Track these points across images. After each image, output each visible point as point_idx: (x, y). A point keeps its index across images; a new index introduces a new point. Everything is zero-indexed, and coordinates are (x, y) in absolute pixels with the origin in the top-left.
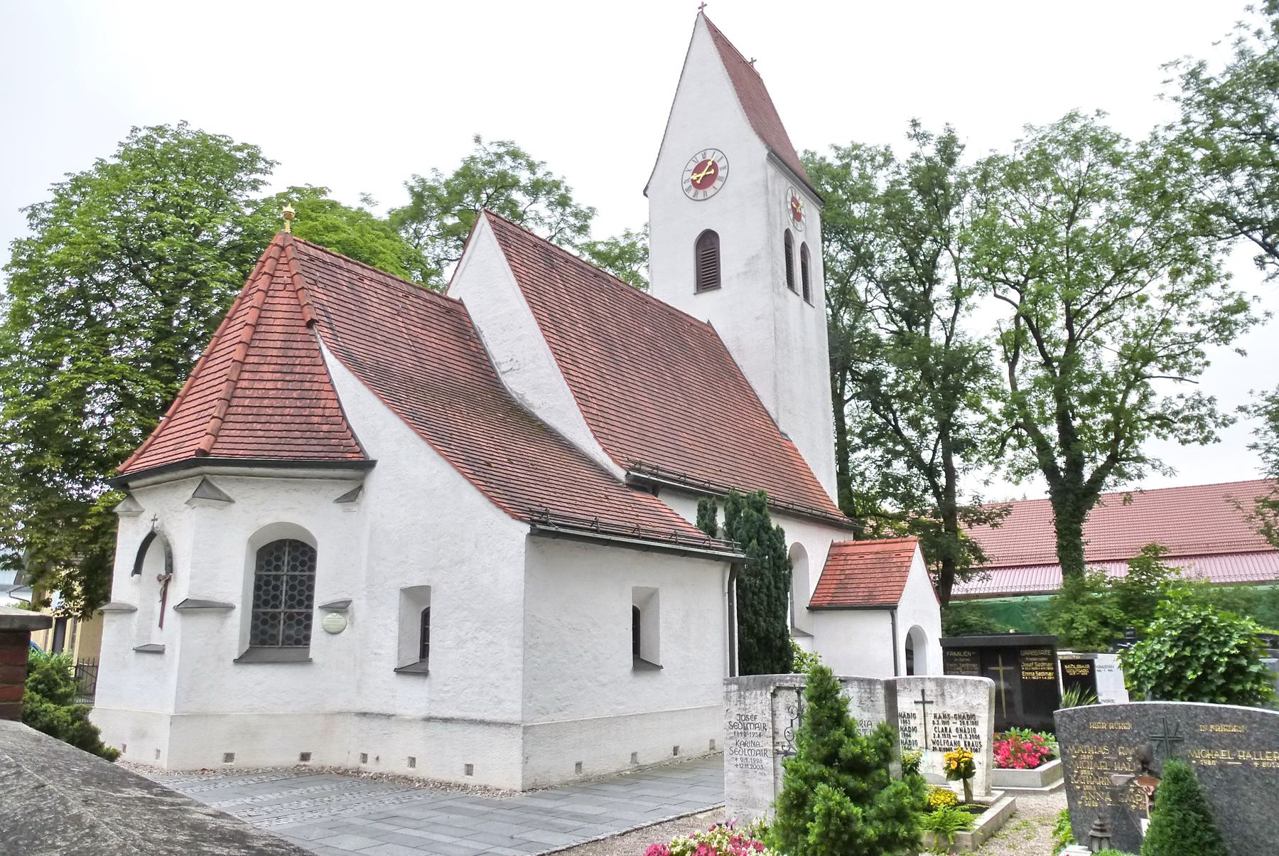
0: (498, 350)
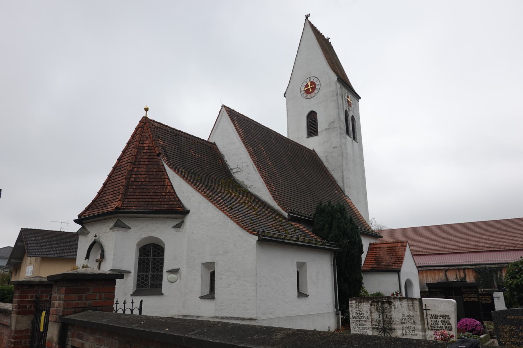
0: (232, 162)
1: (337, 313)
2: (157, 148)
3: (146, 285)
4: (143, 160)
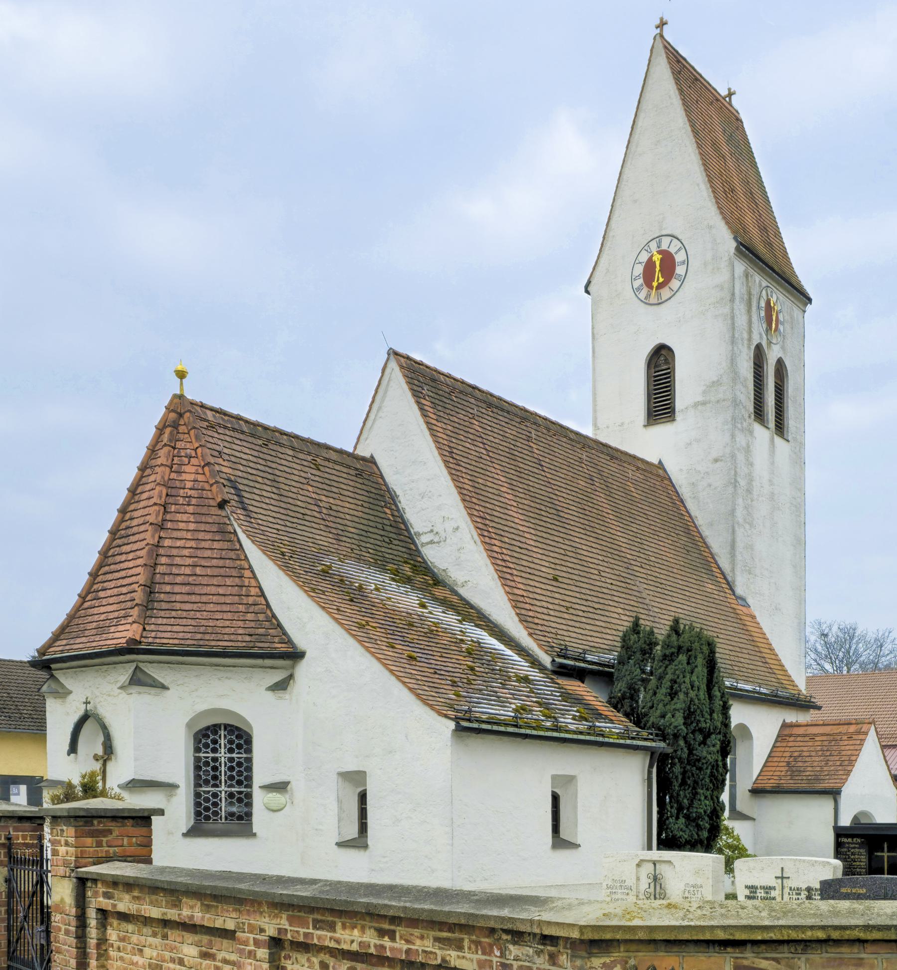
3: (216, 813)
4: (185, 519)
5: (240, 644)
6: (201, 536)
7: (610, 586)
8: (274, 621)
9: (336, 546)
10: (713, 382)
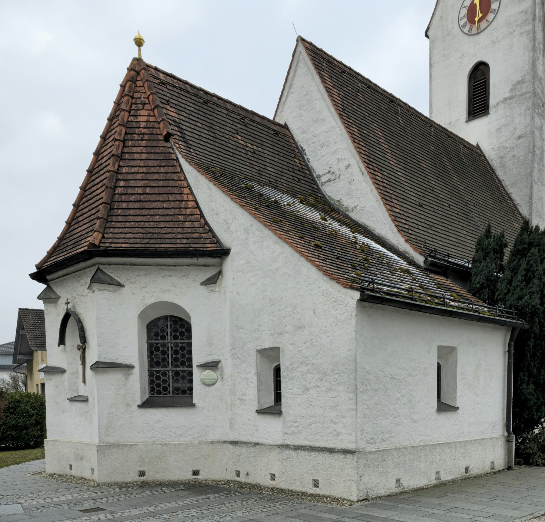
1: (508, 438)
2: (163, 123)
3: (165, 389)
4: (139, 151)
5: (178, 246)
6: (151, 163)
7: (457, 216)
8: (206, 227)
9: (258, 178)
10: (519, 82)
